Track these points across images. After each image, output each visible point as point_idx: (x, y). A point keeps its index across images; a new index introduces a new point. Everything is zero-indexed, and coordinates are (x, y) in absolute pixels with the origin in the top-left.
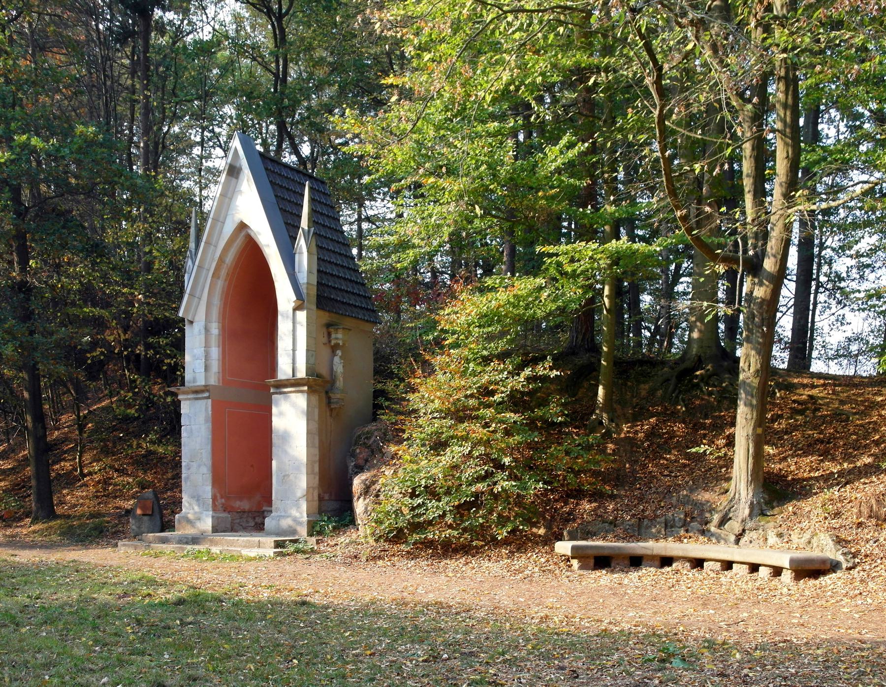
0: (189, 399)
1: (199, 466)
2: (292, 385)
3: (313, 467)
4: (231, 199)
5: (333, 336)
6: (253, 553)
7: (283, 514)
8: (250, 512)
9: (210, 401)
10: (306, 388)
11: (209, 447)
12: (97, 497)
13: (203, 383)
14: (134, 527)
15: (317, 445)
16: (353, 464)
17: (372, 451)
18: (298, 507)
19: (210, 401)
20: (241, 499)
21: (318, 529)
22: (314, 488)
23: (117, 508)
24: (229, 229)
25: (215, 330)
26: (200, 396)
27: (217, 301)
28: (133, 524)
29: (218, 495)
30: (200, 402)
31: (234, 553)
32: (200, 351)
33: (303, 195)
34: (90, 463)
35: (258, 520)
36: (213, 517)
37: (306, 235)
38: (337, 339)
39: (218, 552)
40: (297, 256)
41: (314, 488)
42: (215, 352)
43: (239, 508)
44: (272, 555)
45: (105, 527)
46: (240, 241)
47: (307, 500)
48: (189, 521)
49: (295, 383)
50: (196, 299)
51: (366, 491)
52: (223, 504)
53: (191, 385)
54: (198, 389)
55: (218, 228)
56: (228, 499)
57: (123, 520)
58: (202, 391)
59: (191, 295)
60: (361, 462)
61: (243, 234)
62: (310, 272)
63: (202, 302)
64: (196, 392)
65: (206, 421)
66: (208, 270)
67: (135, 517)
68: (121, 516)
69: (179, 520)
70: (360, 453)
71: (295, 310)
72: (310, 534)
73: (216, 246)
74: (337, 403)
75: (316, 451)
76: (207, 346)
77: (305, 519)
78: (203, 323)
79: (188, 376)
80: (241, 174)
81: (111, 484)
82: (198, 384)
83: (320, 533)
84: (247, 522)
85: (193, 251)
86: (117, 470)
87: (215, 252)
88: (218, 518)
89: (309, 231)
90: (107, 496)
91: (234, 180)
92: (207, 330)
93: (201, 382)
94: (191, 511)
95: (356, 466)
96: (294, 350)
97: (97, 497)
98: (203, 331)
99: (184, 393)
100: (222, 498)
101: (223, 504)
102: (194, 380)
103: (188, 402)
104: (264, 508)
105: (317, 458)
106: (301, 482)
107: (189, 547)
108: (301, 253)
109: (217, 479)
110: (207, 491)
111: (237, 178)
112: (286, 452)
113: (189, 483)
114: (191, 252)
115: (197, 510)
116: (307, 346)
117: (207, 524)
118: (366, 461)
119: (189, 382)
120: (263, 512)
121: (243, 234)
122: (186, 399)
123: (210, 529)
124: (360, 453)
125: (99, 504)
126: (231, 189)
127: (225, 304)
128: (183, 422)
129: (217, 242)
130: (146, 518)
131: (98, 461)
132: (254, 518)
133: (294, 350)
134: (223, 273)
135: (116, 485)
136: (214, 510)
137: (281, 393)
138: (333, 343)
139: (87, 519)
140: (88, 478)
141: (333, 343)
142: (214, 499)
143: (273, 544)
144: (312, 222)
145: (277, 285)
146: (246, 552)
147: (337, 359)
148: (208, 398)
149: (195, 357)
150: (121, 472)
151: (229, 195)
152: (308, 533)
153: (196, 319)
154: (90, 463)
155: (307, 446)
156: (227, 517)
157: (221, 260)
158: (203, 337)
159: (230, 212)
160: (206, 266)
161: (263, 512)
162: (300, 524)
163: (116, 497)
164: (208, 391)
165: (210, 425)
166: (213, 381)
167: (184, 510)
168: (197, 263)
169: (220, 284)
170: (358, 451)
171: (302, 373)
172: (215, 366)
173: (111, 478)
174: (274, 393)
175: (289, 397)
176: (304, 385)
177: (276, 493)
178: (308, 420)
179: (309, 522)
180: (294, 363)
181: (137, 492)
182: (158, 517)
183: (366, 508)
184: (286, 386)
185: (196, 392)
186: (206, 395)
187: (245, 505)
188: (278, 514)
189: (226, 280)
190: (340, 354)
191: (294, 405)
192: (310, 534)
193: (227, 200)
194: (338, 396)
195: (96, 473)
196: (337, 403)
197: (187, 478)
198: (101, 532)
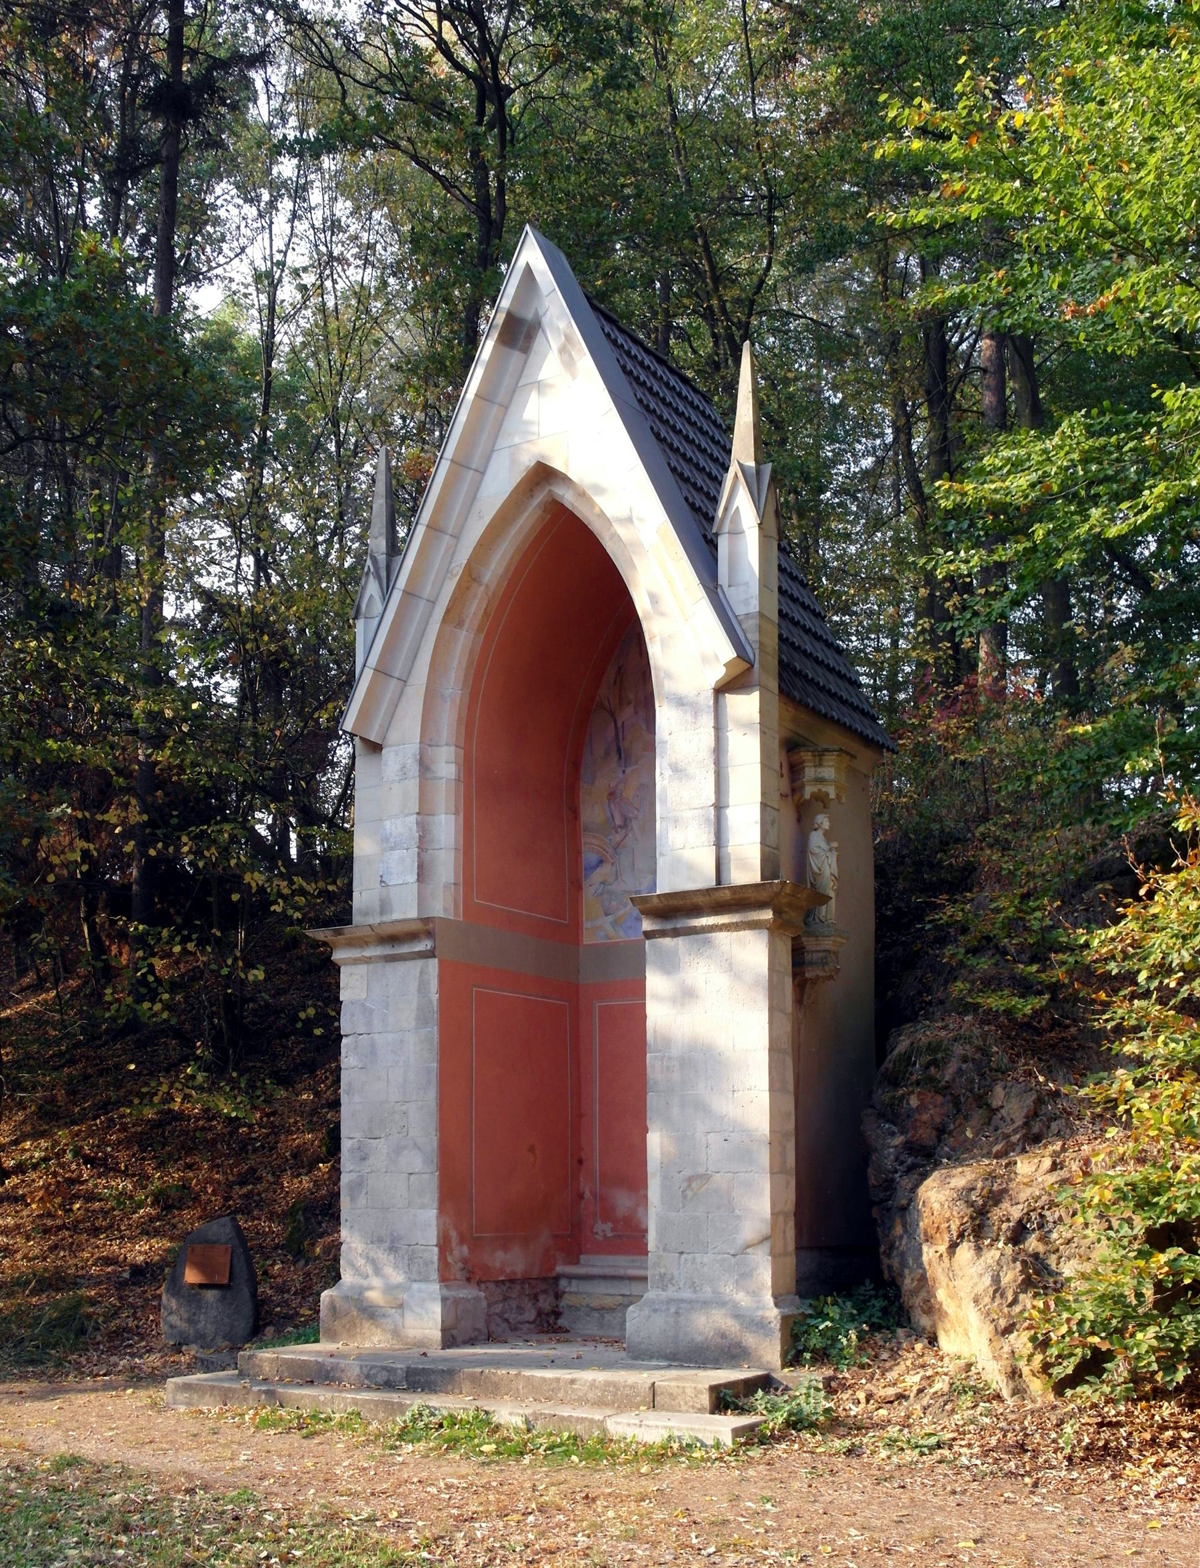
0: (368, 961)
1: (398, 1150)
2: (719, 908)
3: (783, 1153)
4: (506, 407)
5: (810, 773)
6: (650, 1429)
7: (687, 1294)
8: (525, 1280)
9: (433, 964)
10: (767, 915)
11: (432, 1095)
12: (46, 1231)
13: (413, 914)
14: (174, 1319)
15: (791, 1087)
16: (898, 1140)
17: (956, 1103)
18: (745, 1276)
19: (433, 964)
20: (506, 1248)
21: (815, 1341)
22: (786, 1215)
23: (108, 1261)
24: (499, 483)
25: (446, 766)
26: (405, 949)
27: (453, 689)
28: (172, 1314)
29: (453, 1234)
30: (401, 967)
31: (580, 1429)
32: (403, 826)
33: (731, 388)
34: (16, 1143)
35: (546, 1303)
36: (444, 1300)
37: (753, 480)
38: (821, 780)
39: (519, 1422)
40: (723, 543)
41: (786, 1215)
42: (446, 828)
43: (502, 1271)
44: (727, 1440)
45: (89, 1317)
46: (528, 518)
47: (773, 1254)
48: (370, 1313)
49: (726, 900)
50: (393, 684)
51: (977, 1227)
52: (465, 1261)
53: (375, 920)
54: (399, 929)
55: (465, 487)
56: (476, 1244)
57: (133, 1295)
58: (413, 936)
59: (382, 671)
60: (926, 1135)
61: (539, 498)
62: (763, 584)
63: (409, 691)
64: (392, 939)
65: (422, 1020)
66: (433, 603)
67: (177, 1287)
68: (122, 1285)
69: (333, 1308)
70: (922, 1108)
71: (721, 690)
72: (793, 1359)
73: (456, 537)
74: (823, 963)
75: (789, 1104)
76: (424, 812)
77: (773, 1314)
78: (413, 748)
79: (363, 896)
80: (539, 340)
81: (76, 1197)
82: (396, 916)
83: (821, 1357)
84: (520, 1309)
85: (382, 558)
86: (88, 1160)
87: (452, 552)
88: (457, 1301)
89: (758, 472)
90: (74, 1228)
91: (516, 356)
92: (424, 766)
93: (406, 909)
94: (376, 1282)
95: (910, 1147)
96: (719, 807)
97: (46, 1231)
98: (414, 770)
99: (352, 943)
100: (462, 1241)
101: (465, 1261)
102: (385, 906)
103: (362, 969)
104: (559, 1269)
105: (791, 1125)
106: (757, 1202)
107: (415, 1402)
108: (736, 532)
109: (453, 1192)
110: (424, 1222)
111: (526, 350)
112: (702, 1108)
113: (362, 1201)
114: (375, 561)
115: (390, 1272)
116: (763, 794)
117: (425, 1321)
118: (941, 1131)
119: (366, 914)
120: (557, 1278)
121: (539, 498)
122: (356, 961)
123: (437, 1335)
124: (922, 1108)
125: (54, 1248)
126: (507, 382)
127: (473, 696)
128: (345, 1025)
129: (462, 526)
130: (211, 1295)
131: (36, 1135)
132: (535, 1298)
133: (719, 807)
134: (475, 608)
135: (91, 1197)
136: (443, 1279)
137: (676, 933)
138: (808, 791)
139: (33, 1293)
140: (15, 1180)
141: (808, 791)
142: (444, 1245)
143: (705, 1400)
144: (763, 446)
145: (654, 629)
146: (627, 1427)
147: (817, 840)
148: (430, 954)
149: (387, 843)
150: (102, 1165)
151: (501, 397)
152: (784, 1354)
153: (393, 736)
154: (16, 1143)
155: (771, 1089)
156: (477, 1299)
157: (471, 575)
158: (413, 786)
159: (502, 442)
160: (427, 592)
161: (557, 1278)
162: (760, 1326)
163: (95, 1231)
164: (429, 934)
165: (433, 1031)
166: (441, 906)
167: (347, 1277)
168: (402, 583)
169: (464, 641)
170: (914, 1102)
171: (746, 869)
172: (446, 866)
173: (73, 1182)
174: (649, 935)
175: (708, 942)
176: (761, 905)
177: (662, 1232)
178: (771, 1010)
179: (785, 1319)
180: (719, 842)
181: (152, 1219)
182: (246, 1292)
183: (996, 1280)
184: (697, 911)
185: (392, 939)
186: (424, 945)
187: (512, 1260)
188: (671, 1293)
189: (479, 630)
190: (827, 825)
191: (731, 968)
192: (793, 1359)
193: (494, 410)
194: (827, 944)
195: (35, 1167)
196: (823, 963)
197: (359, 1184)
198: (82, 1331)
